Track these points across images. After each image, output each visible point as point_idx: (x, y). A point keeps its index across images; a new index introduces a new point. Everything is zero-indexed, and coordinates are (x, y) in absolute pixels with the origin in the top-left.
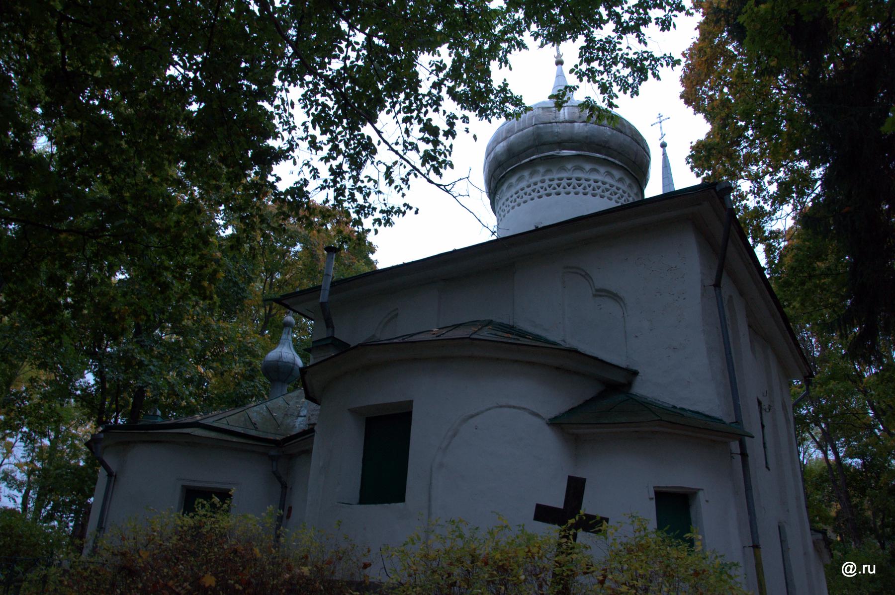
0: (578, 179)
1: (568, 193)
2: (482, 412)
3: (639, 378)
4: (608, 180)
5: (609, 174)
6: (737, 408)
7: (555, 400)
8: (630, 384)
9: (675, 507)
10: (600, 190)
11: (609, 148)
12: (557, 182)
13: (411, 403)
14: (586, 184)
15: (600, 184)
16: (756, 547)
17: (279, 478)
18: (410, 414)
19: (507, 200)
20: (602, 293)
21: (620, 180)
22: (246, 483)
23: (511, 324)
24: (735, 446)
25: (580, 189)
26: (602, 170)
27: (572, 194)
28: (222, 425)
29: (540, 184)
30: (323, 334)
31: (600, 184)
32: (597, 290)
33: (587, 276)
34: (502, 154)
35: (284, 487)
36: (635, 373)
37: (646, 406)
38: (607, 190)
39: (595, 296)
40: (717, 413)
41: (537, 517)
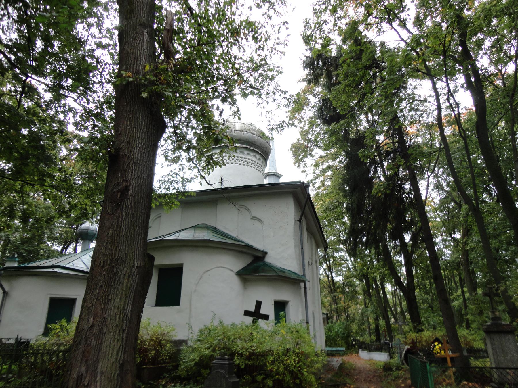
0: (241, 158)
1: (236, 164)
4: (254, 159)
5: (255, 156)
6: (304, 270)
7: (237, 264)
8: (264, 257)
9: (280, 306)
13: (182, 265)
14: (245, 160)
15: (250, 161)
20: (254, 218)
21: (259, 159)
23: (215, 226)
24: (302, 284)
25: (242, 162)
26: (252, 154)
28: (70, 266)
33: (248, 210)
36: (266, 253)
37: (270, 268)
38: (253, 164)
40: (297, 272)
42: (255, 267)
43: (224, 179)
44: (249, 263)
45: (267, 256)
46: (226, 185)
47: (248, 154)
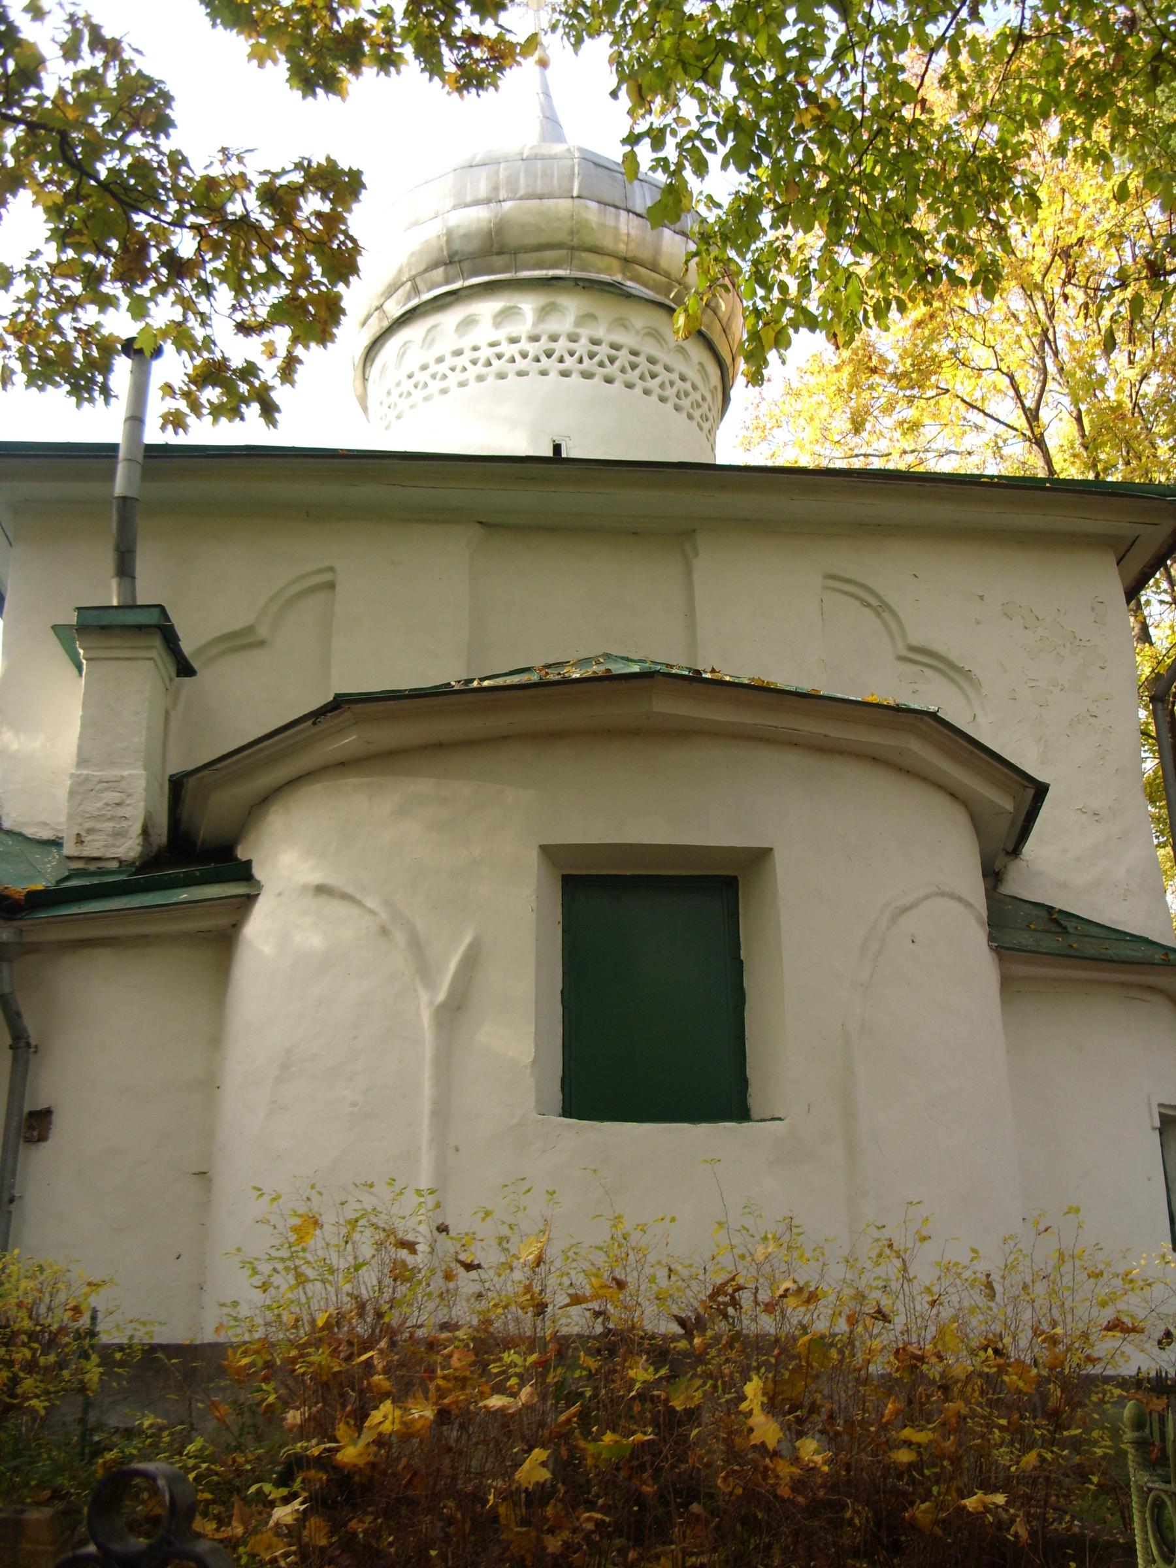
13: (760, 857)
32: (912, 649)
34: (466, 236)
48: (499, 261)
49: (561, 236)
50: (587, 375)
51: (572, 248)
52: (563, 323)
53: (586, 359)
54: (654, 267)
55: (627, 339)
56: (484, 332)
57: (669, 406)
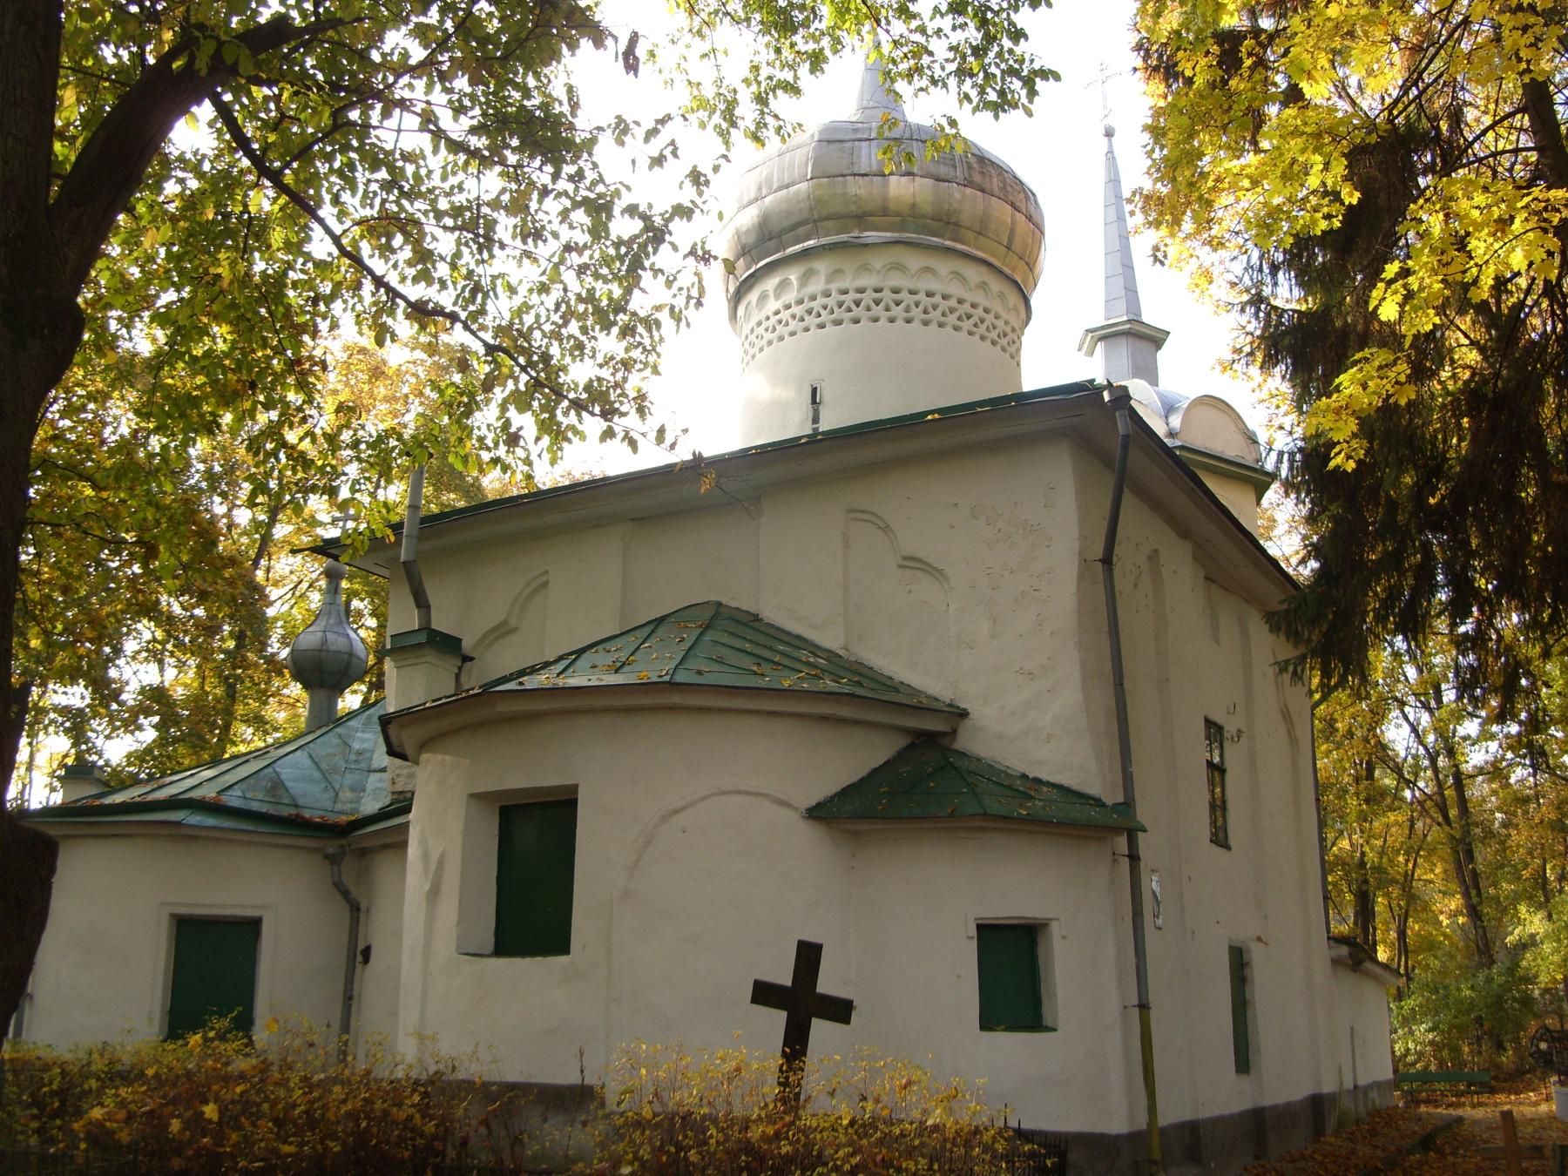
0: (896, 291)
1: (876, 320)
2: (693, 804)
3: (967, 723)
4: (956, 290)
10: (939, 312)
11: (957, 225)
12: (852, 296)
13: (575, 788)
15: (937, 299)
16: (1143, 1006)
17: (346, 894)
18: (573, 803)
19: (759, 324)
20: (911, 562)
22: (275, 895)
24: (1122, 843)
25: (897, 311)
27: (883, 321)
29: (821, 300)
30: (406, 619)
31: (937, 299)
32: (905, 558)
34: (747, 231)
35: (355, 909)
36: (964, 714)
38: (952, 310)
39: (900, 566)
40: (1094, 790)
41: (803, 946)
42: (919, 779)
43: (826, 394)
44: (877, 764)
45: (965, 728)
46: (830, 421)
47: (928, 270)
48: (772, 244)
49: (805, 214)
50: (838, 323)
51: (815, 221)
52: (817, 286)
53: (836, 309)
54: (885, 212)
55: (868, 281)
56: (773, 305)
57: (916, 324)
